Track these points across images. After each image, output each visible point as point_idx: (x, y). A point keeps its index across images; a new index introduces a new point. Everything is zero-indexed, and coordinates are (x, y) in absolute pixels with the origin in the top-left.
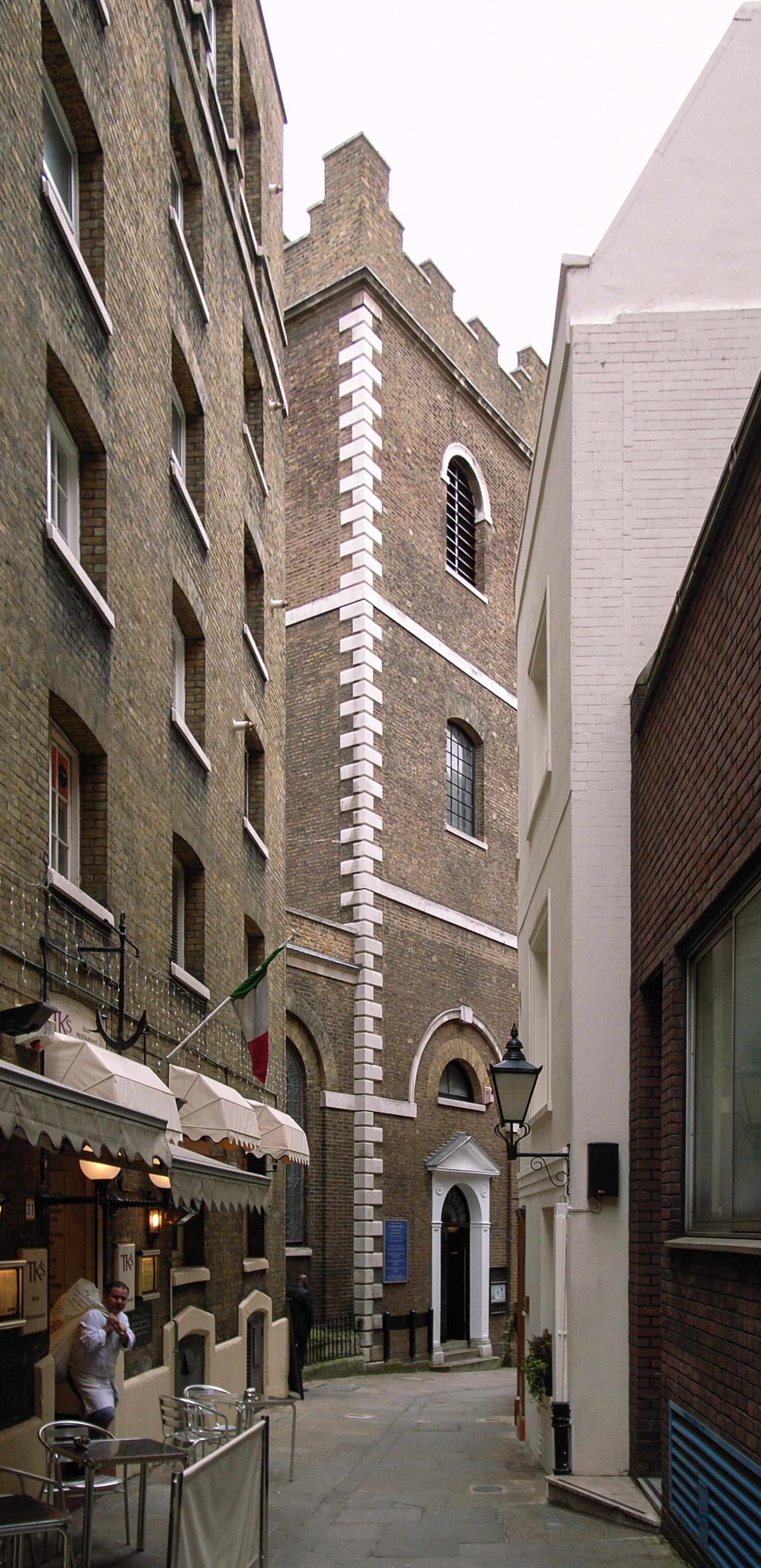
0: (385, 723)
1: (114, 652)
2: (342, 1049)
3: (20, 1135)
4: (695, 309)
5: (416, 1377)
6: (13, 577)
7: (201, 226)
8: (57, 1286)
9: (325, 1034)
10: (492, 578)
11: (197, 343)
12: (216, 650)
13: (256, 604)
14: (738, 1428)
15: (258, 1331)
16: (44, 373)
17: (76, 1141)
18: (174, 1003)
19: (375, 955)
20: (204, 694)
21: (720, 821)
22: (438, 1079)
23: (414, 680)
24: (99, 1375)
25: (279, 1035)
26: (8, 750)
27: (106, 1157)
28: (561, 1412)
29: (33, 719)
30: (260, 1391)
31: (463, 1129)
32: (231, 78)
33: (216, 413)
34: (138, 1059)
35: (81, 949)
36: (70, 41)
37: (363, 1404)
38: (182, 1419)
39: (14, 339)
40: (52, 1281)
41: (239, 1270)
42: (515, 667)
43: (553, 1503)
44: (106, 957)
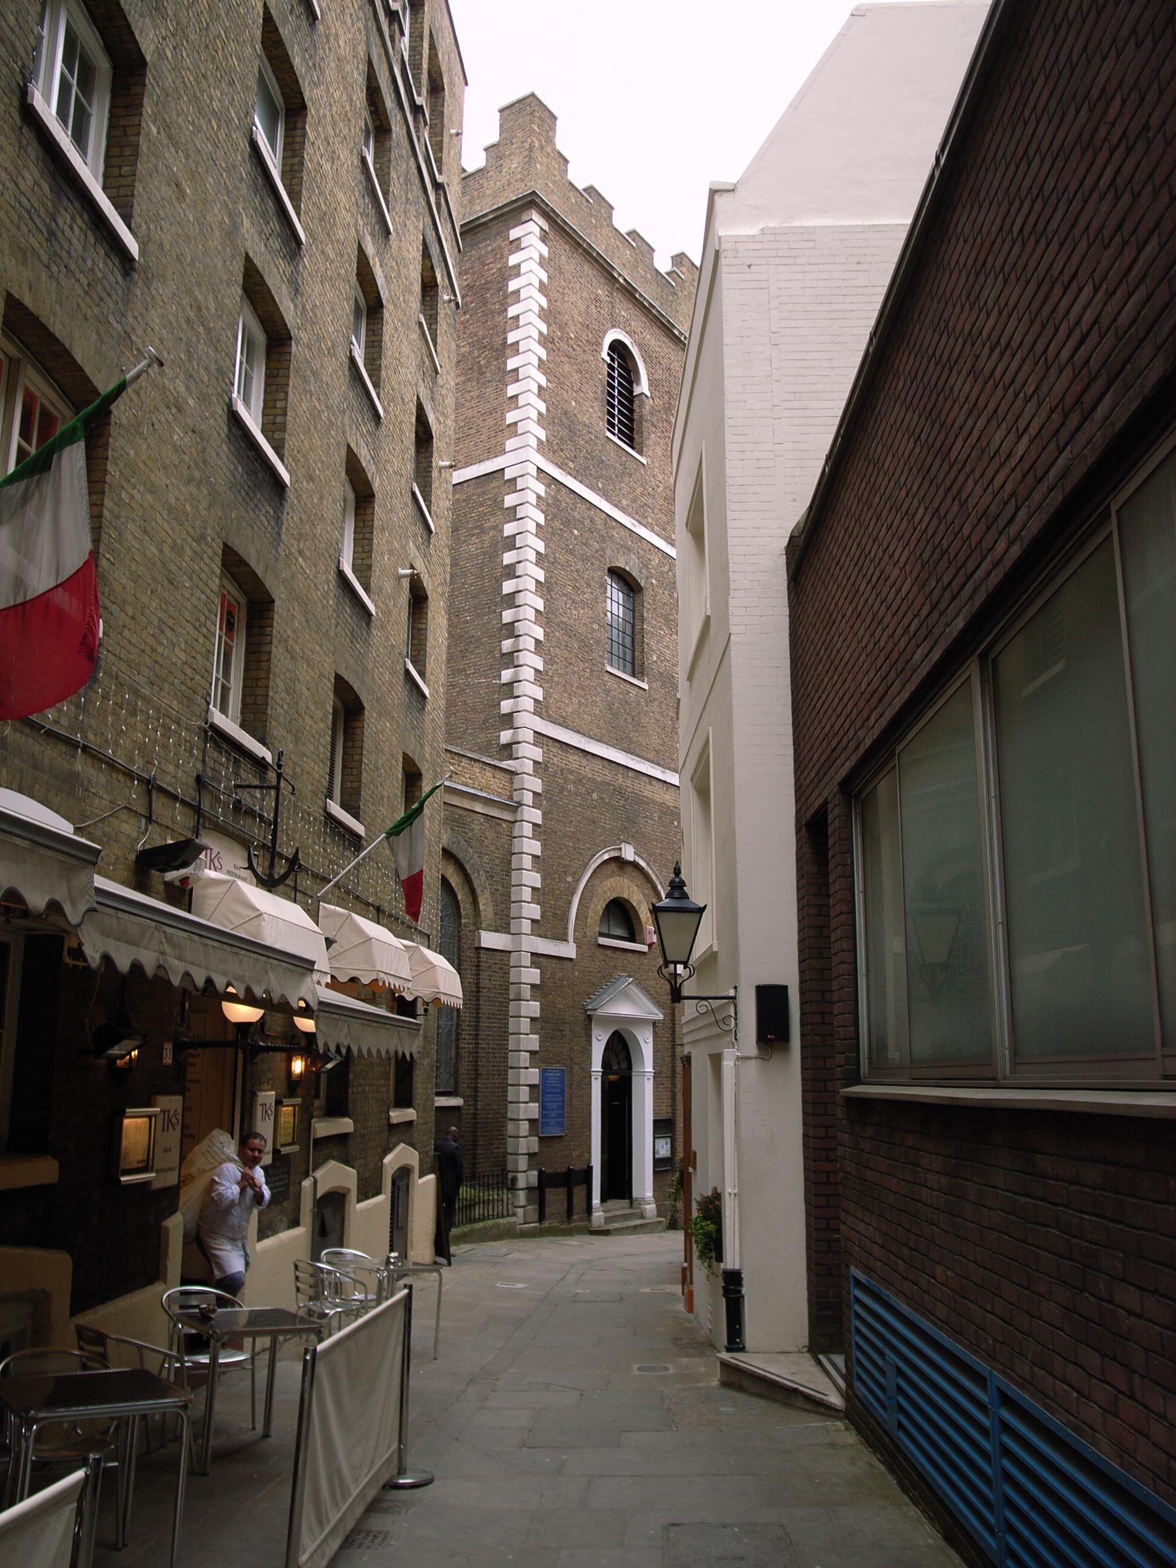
0: (547, 571)
1: (287, 508)
2: (499, 887)
3: (162, 974)
4: (831, 224)
5: (574, 1241)
6: (198, 443)
7: (389, 161)
8: (191, 1137)
9: (481, 872)
10: (650, 442)
11: (381, 251)
12: (385, 506)
13: (425, 465)
14: (926, 1296)
15: (403, 1188)
16: (241, 276)
17: (220, 982)
18: (328, 840)
19: (534, 793)
20: (371, 545)
21: (879, 662)
22: (598, 918)
23: (576, 532)
24: (230, 1235)
25: (433, 871)
26: (179, 597)
27: (249, 999)
28: (733, 1280)
29: (205, 568)
30: (404, 1256)
31: (624, 971)
32: (421, 54)
33: (395, 305)
34: (288, 898)
35: (237, 786)
36: (285, 31)
37: (519, 1269)
38: (318, 1286)
39: (217, 249)
40: (186, 1132)
41: (385, 1121)
42: (673, 520)
43: (725, 1384)
44: (262, 794)
